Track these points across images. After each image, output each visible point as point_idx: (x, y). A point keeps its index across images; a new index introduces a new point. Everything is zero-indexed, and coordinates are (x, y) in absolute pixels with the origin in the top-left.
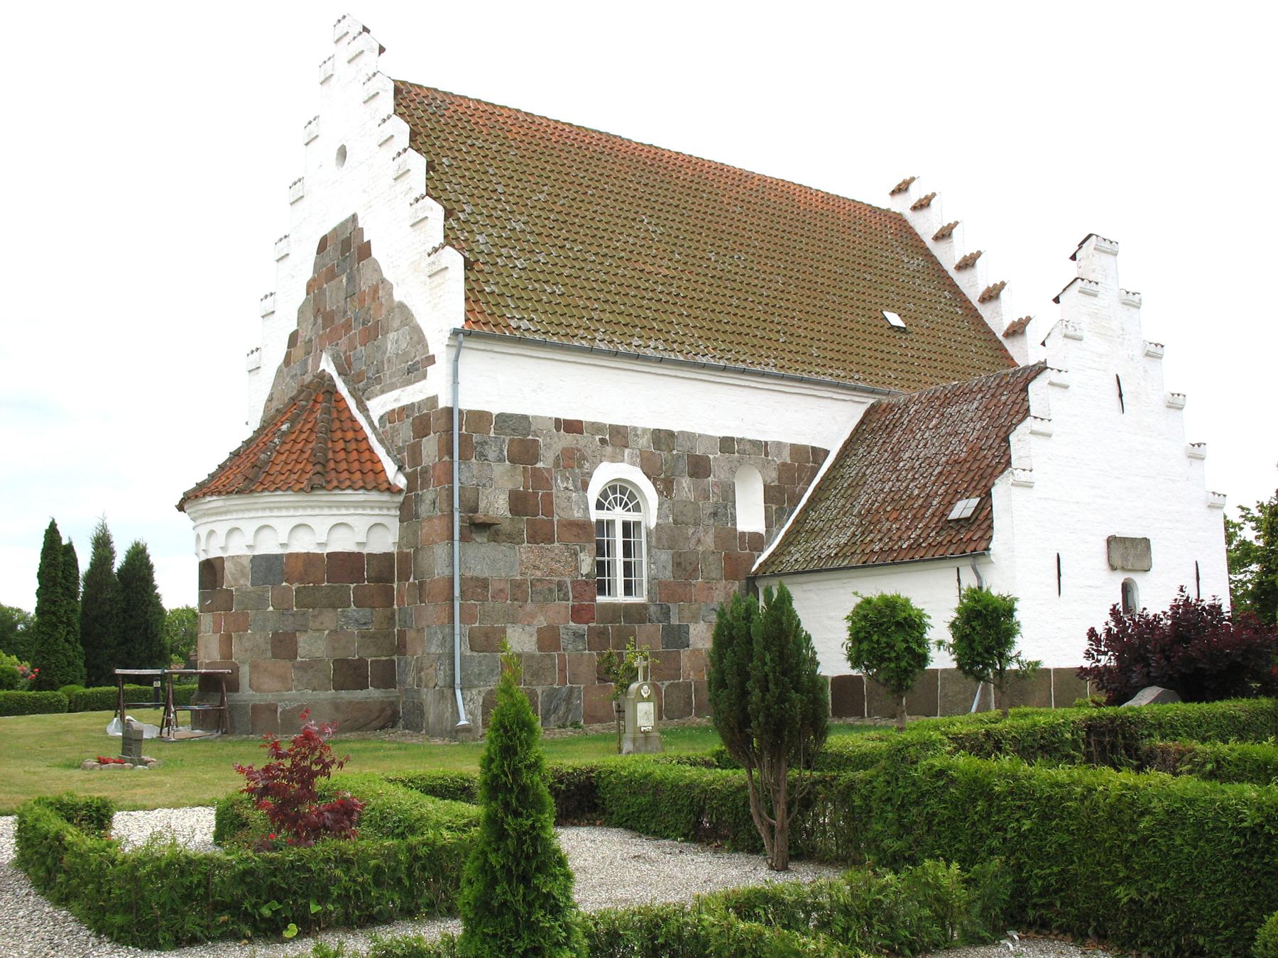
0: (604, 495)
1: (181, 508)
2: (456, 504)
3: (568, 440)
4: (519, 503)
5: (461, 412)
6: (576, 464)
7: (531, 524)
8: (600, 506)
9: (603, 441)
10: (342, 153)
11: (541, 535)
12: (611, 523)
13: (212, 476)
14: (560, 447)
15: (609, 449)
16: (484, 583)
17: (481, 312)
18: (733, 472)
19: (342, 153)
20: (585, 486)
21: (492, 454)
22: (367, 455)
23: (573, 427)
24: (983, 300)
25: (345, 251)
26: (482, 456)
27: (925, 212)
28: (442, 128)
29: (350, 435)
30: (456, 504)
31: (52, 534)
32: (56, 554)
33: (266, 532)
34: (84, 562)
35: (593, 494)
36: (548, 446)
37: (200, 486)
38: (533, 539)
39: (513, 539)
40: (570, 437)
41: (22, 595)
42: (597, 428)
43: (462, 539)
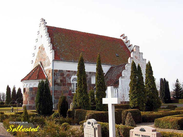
0: (73, 80)
1: (22, 80)
2: (53, 81)
3: (68, 73)
4: (61, 81)
5: (54, 70)
6: (69, 76)
7: (63, 84)
8: (72, 81)
9: (73, 73)
10: (42, 36)
11: (64, 85)
12: (74, 83)
13: (25, 78)
14: (67, 74)
15: (74, 74)
16: (57, 91)
17: (57, 57)
18: (91, 76)
19: (42, 36)
20: (70, 79)
21: (58, 75)
22: (41, 70)
23: (69, 71)
24: (129, 47)
25: (42, 49)
26: (57, 75)
27: (130, 47)
28: (54, 33)
29: (42, 72)
30: (53, 81)
31: (8, 86)
32: (8, 89)
33: (31, 85)
34: (12, 90)
35: (71, 81)
36: (65, 74)
37: (23, 79)
38: (63, 85)
39: (61, 85)
40: (68, 72)
41: (5, 91)
42: (72, 71)
43: (54, 85)
